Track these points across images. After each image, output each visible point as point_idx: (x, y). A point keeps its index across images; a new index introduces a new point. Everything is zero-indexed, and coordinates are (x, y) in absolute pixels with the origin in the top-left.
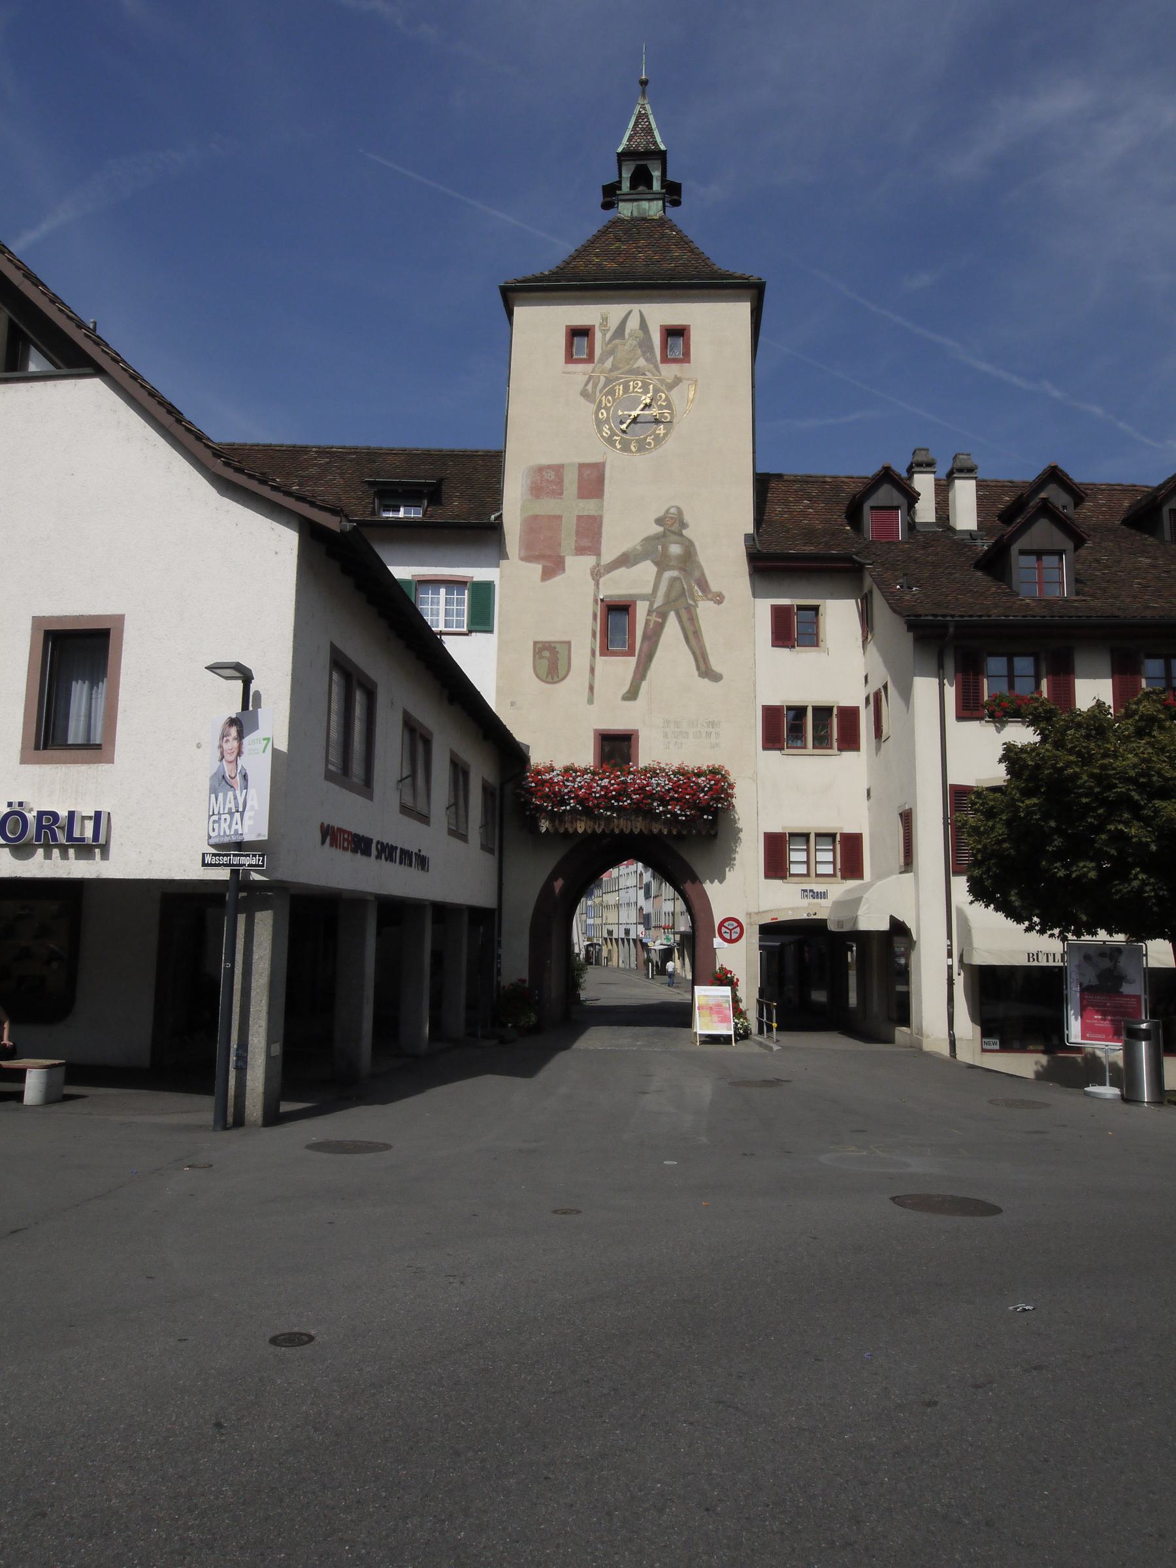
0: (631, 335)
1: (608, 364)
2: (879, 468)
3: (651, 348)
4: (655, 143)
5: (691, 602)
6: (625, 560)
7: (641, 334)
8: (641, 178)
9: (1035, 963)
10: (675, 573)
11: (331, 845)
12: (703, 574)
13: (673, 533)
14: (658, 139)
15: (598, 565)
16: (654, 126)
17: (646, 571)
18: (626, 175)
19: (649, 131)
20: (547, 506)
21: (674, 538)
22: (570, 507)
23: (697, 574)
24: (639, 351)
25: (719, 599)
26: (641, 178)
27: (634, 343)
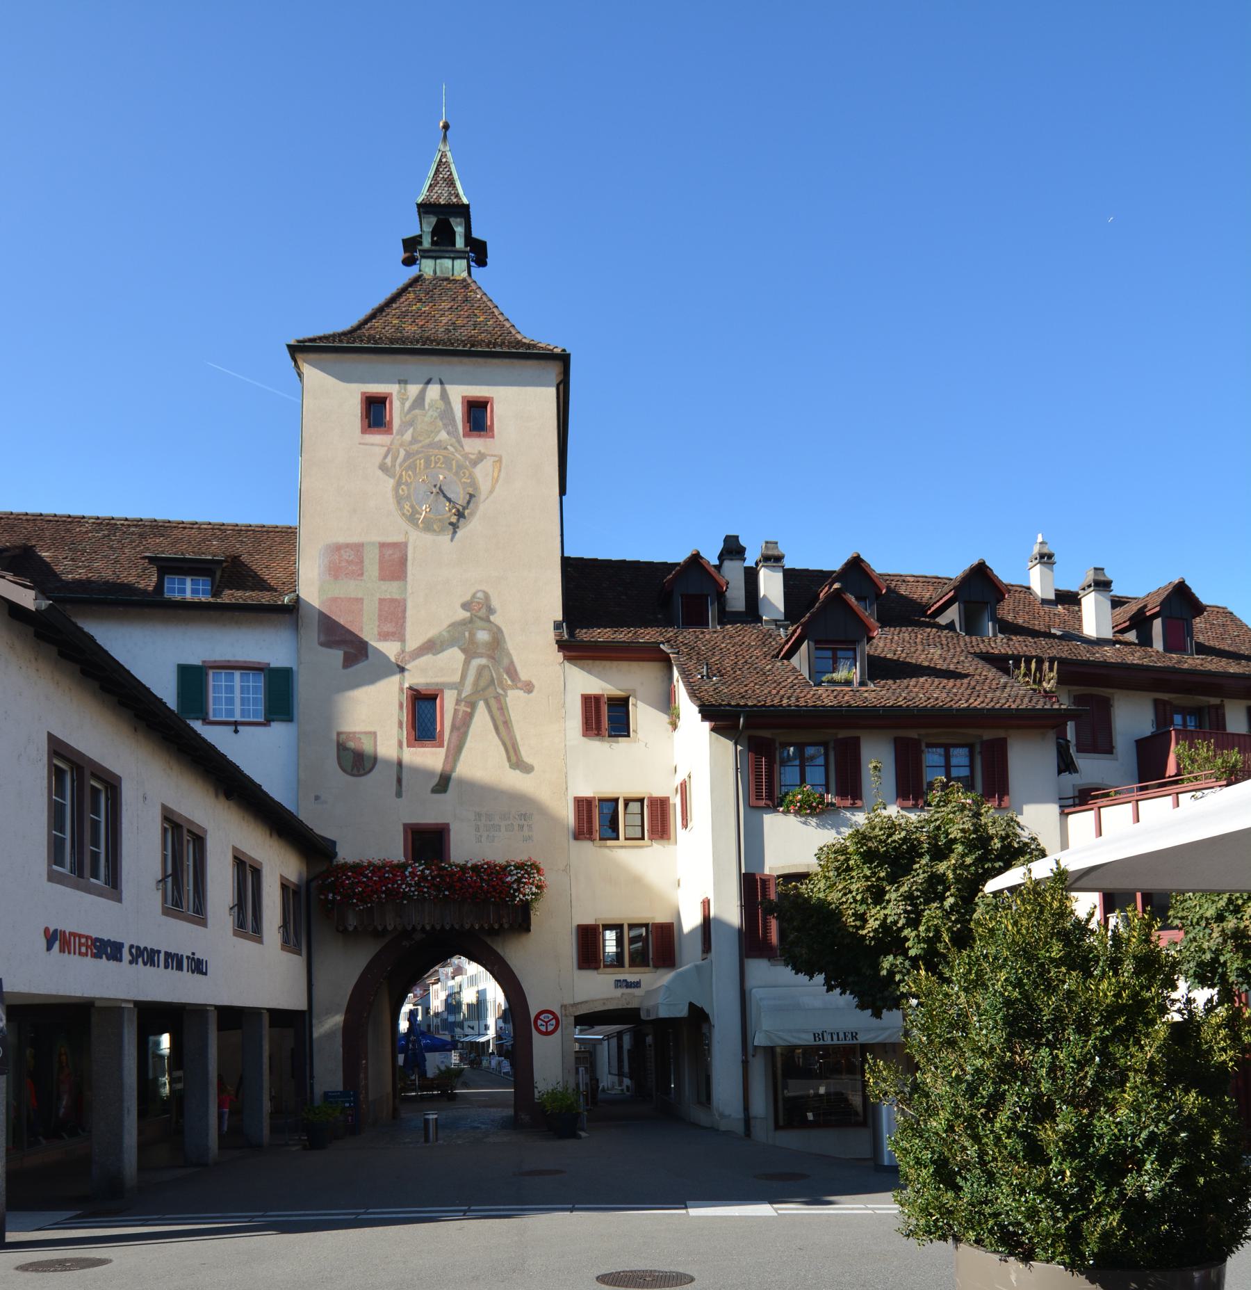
0: (431, 406)
1: (408, 436)
2: (688, 554)
3: (454, 420)
4: (457, 196)
5: (501, 692)
6: (431, 647)
7: (441, 405)
8: (443, 235)
9: (821, 1042)
10: (483, 661)
11: (62, 950)
12: (512, 663)
13: (481, 618)
14: (461, 192)
15: (403, 651)
16: (456, 176)
17: (453, 657)
18: (428, 229)
19: (451, 182)
21: (480, 623)
23: (506, 662)
24: (440, 424)
25: (529, 688)
26: (443, 235)
27: (436, 414)
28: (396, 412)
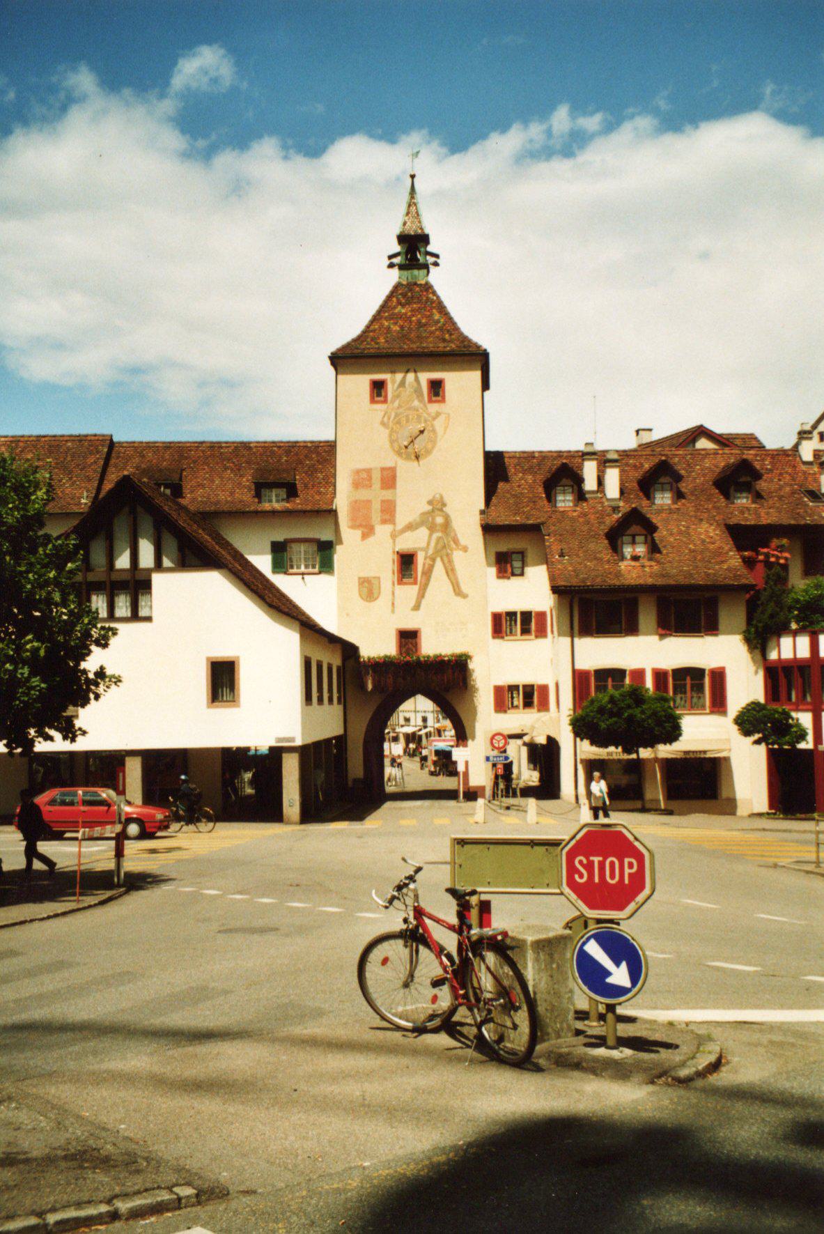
6: (410, 527)
17: (423, 532)
20: (364, 494)
22: (376, 494)
28: (390, 389)
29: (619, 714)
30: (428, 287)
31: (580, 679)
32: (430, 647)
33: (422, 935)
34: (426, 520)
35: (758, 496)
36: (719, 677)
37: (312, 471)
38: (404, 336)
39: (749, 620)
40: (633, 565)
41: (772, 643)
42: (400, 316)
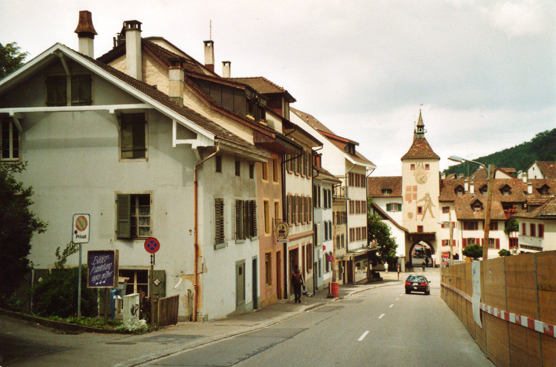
6: (421, 200)
17: (424, 202)
20: (409, 192)
22: (412, 192)
28: (416, 166)
29: (473, 251)
30: (424, 139)
31: (464, 240)
32: (426, 230)
33: (143, 304)
34: (425, 199)
35: (510, 193)
36: (498, 241)
37: (395, 185)
38: (418, 153)
39: (506, 226)
40: (477, 214)
41: (511, 233)
42: (418, 147)
